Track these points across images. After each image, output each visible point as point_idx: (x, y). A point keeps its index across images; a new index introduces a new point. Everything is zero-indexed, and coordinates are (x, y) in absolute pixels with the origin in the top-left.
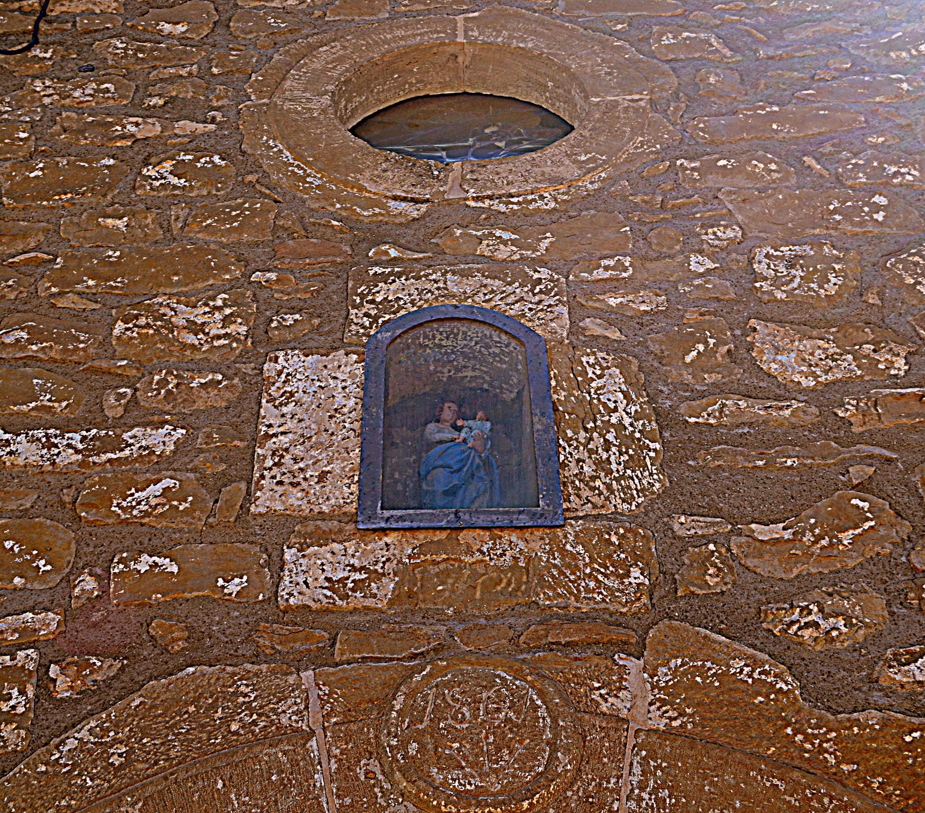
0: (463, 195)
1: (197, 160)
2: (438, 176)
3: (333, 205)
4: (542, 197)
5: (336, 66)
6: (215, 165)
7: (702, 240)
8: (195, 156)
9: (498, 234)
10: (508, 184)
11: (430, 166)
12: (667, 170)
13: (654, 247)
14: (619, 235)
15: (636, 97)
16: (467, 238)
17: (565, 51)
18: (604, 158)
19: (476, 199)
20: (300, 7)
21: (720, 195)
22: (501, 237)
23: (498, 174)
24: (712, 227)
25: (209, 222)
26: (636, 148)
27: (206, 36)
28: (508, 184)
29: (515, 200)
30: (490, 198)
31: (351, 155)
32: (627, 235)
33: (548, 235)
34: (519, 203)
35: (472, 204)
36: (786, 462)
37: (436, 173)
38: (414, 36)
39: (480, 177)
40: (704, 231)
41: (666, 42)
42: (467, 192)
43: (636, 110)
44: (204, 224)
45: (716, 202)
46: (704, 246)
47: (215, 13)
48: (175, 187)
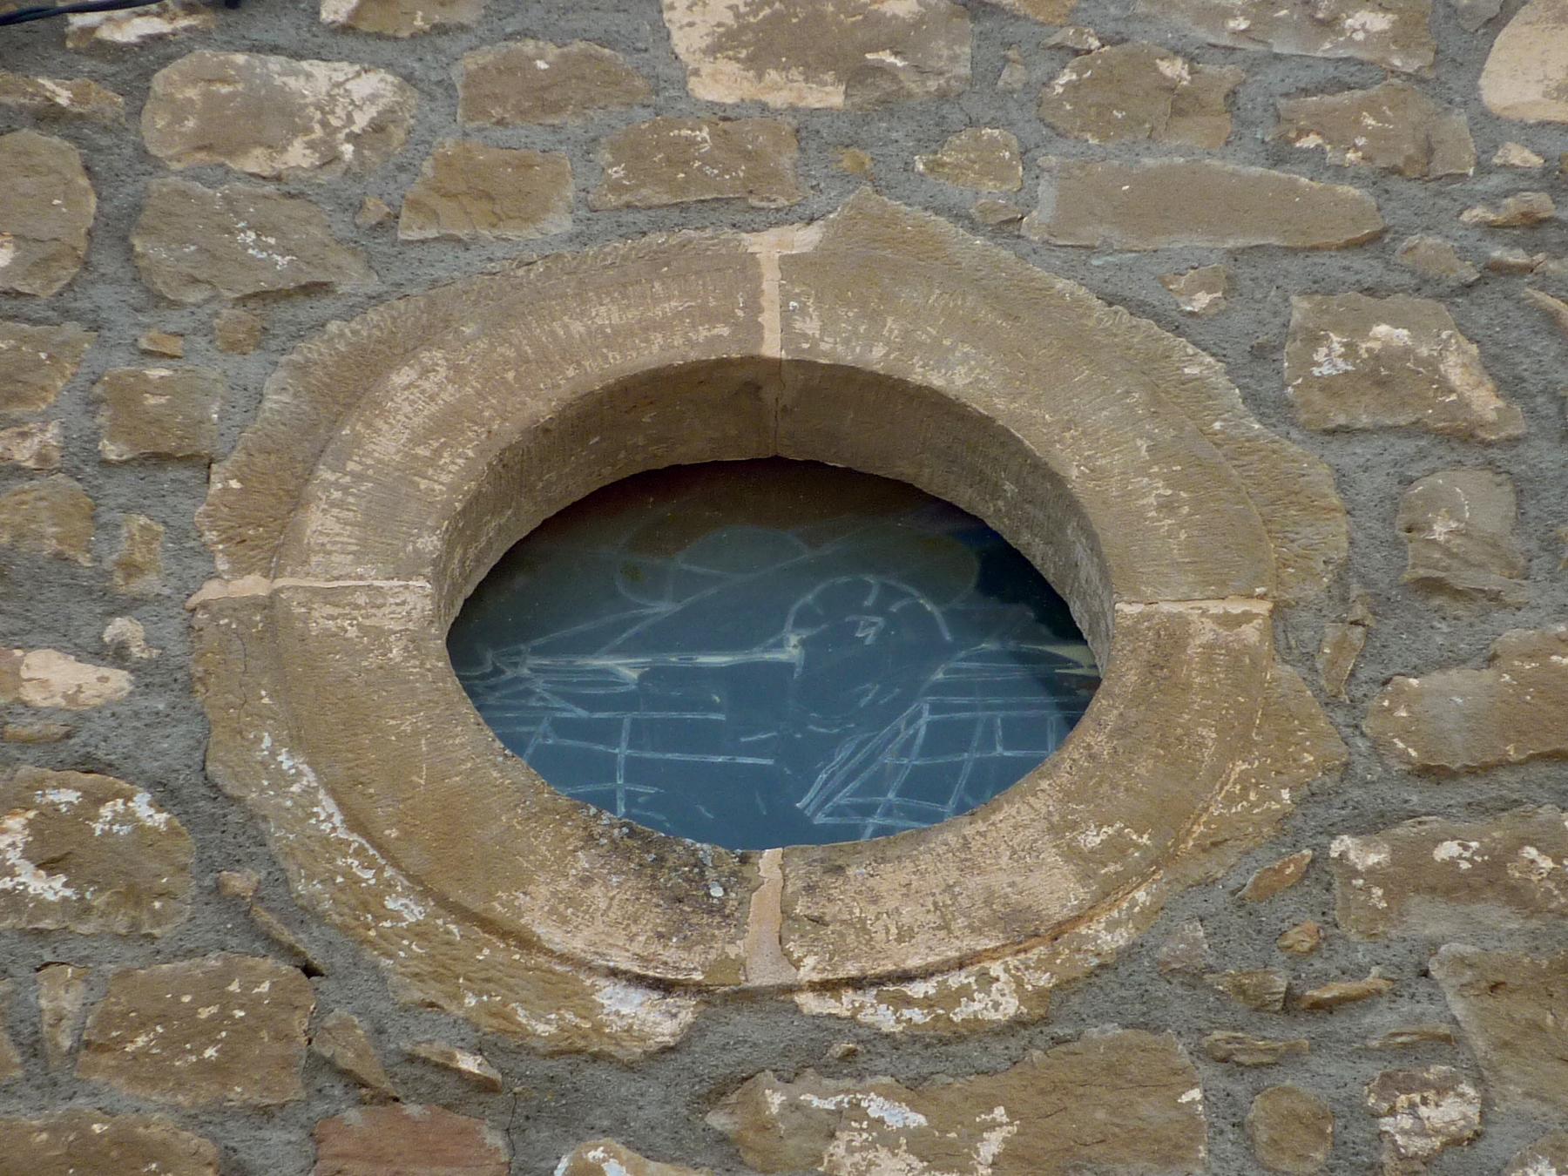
0: (787, 977)
1: (95, 800)
2: (723, 903)
3: (457, 997)
4: (986, 980)
5: (437, 453)
6: (140, 829)
7: (1381, 1135)
8: (86, 793)
9: (874, 1112)
10: (900, 939)
11: (699, 864)
12: (1305, 875)
13: (1261, 1153)
14: (1173, 1114)
15: (1236, 608)
16: (797, 1118)
17: (1054, 411)
18: (1145, 839)
19: (827, 987)
20: (323, 178)
21: (1433, 966)
22: (881, 1121)
23: (875, 901)
24: (1409, 1091)
25: (141, 1041)
26: (1231, 800)
27: (69, 286)
28: (900, 939)
29: (918, 989)
30: (857, 983)
31: (497, 818)
32: (1193, 1117)
33: (1000, 1113)
34: (927, 1003)
35: (810, 1003)
36: (1134, 903)
37: (717, 892)
38: (648, 327)
39: (830, 911)
40: (1385, 1106)
41: (1326, 370)
42: (797, 964)
43: (1235, 657)
44: (129, 1048)
45: (1422, 988)
46: (1384, 1158)
47: (84, 182)
48: (43, 907)
